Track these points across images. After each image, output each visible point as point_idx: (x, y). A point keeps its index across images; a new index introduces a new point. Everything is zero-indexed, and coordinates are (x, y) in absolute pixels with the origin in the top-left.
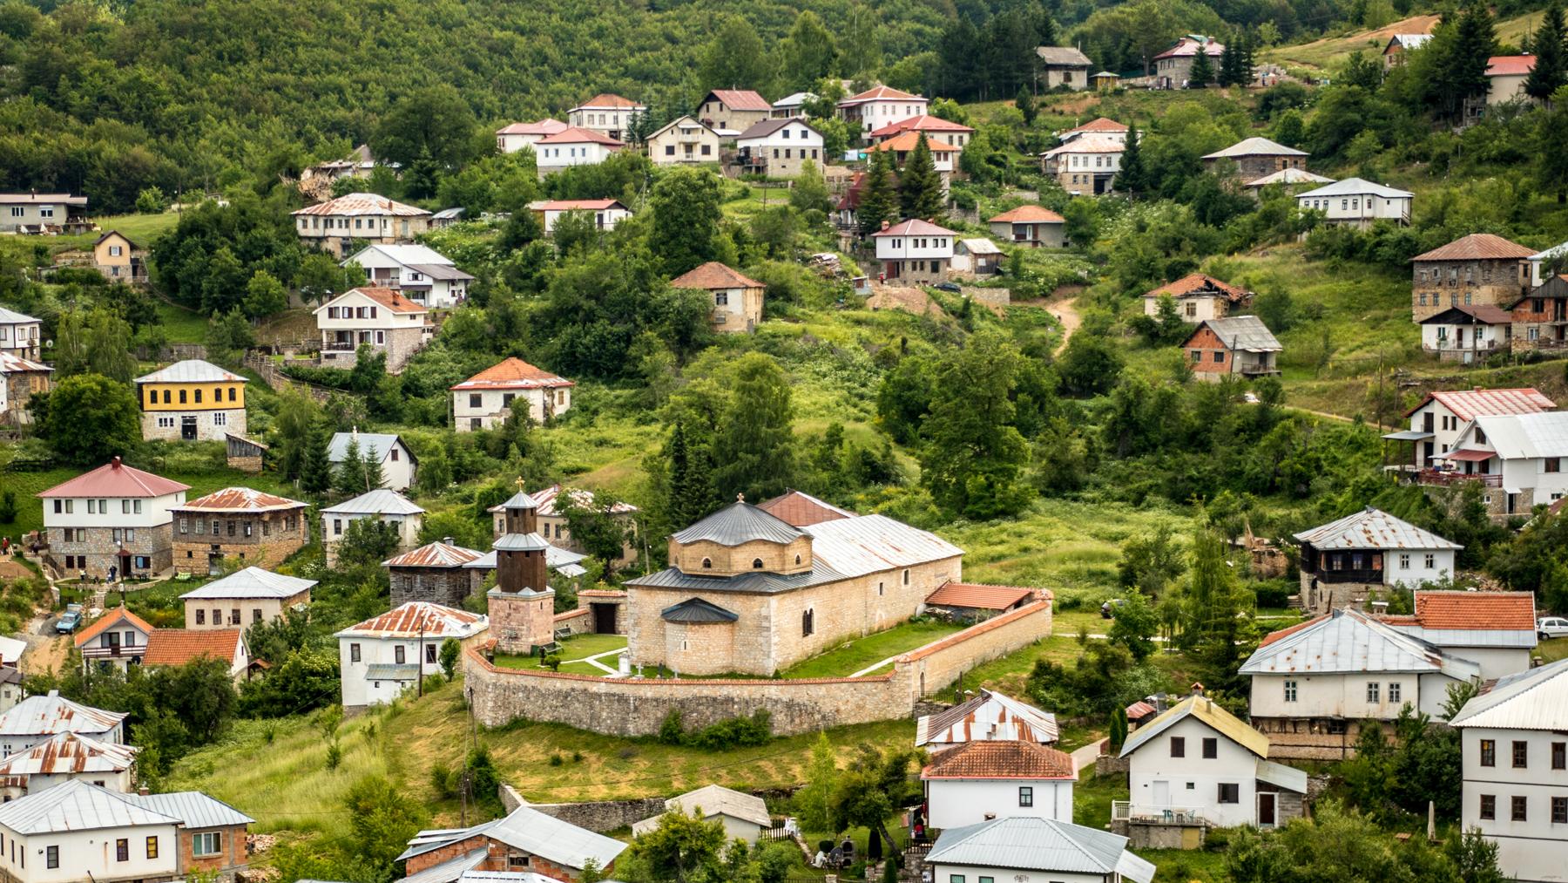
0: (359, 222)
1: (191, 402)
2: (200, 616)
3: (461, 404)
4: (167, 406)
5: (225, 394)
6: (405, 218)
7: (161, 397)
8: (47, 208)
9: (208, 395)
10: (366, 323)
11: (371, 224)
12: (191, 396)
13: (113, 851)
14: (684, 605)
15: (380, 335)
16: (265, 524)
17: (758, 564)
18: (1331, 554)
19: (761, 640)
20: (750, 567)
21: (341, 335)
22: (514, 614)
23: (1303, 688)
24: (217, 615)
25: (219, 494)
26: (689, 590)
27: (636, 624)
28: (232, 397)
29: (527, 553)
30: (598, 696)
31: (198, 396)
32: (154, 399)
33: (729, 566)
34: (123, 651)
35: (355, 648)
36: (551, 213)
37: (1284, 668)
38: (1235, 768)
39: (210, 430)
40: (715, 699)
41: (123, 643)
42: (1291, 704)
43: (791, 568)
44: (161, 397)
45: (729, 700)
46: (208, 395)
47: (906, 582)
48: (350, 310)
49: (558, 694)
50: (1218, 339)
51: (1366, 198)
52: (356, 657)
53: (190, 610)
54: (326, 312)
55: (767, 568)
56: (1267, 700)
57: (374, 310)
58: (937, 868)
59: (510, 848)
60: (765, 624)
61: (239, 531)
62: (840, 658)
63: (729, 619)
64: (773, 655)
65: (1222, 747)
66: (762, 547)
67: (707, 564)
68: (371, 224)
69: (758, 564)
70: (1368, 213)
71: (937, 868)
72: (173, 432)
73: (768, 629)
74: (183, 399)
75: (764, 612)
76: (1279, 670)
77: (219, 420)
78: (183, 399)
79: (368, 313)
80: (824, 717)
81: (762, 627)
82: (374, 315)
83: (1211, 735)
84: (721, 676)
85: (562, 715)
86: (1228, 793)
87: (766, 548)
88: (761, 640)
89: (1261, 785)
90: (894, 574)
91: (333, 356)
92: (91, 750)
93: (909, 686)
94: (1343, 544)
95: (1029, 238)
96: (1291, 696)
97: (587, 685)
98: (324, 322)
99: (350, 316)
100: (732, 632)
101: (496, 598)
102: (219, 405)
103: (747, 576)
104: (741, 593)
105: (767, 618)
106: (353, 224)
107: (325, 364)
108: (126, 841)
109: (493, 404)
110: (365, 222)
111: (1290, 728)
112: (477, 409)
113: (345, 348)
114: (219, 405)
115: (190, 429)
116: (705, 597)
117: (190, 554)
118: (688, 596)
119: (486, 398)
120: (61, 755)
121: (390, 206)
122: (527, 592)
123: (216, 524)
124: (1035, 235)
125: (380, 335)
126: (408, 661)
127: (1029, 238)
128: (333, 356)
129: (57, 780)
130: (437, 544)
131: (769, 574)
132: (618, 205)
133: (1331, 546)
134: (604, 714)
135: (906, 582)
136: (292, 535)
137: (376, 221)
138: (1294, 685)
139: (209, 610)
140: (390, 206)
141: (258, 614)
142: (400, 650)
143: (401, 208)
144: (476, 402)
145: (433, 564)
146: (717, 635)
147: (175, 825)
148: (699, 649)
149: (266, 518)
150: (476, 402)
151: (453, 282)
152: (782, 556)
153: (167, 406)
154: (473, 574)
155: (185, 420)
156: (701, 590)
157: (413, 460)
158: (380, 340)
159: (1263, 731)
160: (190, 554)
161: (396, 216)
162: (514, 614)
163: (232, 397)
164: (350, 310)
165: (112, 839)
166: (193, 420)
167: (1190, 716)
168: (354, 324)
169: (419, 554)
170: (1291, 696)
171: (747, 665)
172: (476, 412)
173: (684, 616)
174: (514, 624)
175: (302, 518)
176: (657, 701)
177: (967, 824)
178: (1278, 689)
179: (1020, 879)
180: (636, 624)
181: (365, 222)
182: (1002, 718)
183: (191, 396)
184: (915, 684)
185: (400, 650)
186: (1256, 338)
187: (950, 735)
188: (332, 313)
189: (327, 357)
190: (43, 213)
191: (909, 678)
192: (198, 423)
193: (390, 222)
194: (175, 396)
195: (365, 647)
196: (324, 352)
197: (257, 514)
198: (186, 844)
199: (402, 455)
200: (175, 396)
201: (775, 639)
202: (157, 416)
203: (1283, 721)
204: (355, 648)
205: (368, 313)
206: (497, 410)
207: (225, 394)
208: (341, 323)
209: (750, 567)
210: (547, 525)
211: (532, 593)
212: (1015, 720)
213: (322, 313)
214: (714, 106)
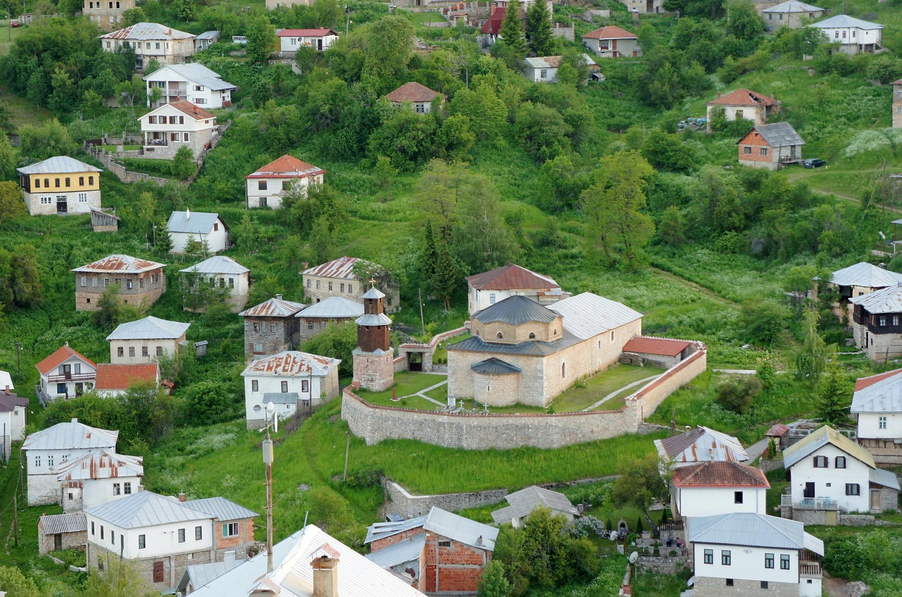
0: (148, 44)
2: (121, 351)
3: (252, 187)
5: (86, 181)
6: (179, 40)
7: (42, 183)
9: (75, 181)
10: (176, 127)
11: (158, 46)
12: (63, 183)
13: (176, 536)
15: (186, 135)
17: (532, 336)
18: (878, 316)
19: (537, 384)
20: (527, 338)
21: (156, 135)
22: (370, 366)
23: (890, 420)
24: (132, 350)
25: (106, 259)
27: (453, 373)
28: (91, 183)
29: (379, 327)
30: (441, 424)
31: (68, 183)
32: (38, 185)
33: (515, 338)
34: (73, 377)
35: (255, 383)
36: (289, 44)
37: (878, 409)
38: (860, 475)
40: (517, 426)
41: (73, 372)
42: (883, 430)
43: (552, 338)
44: (42, 183)
45: (526, 426)
46: (75, 181)
47: (612, 338)
48: (165, 118)
49: (415, 422)
50: (764, 140)
51: (852, 30)
53: (114, 347)
54: (148, 120)
55: (538, 338)
56: (867, 428)
57: (182, 119)
58: (696, 545)
59: (439, 536)
62: (580, 393)
64: (545, 394)
65: (850, 462)
66: (534, 325)
68: (158, 46)
69: (532, 336)
70: (853, 40)
71: (696, 545)
72: (50, 208)
73: (542, 378)
74: (58, 185)
75: (539, 367)
76: (876, 410)
77: (83, 199)
78: (58, 185)
79: (178, 120)
80: (584, 436)
81: (538, 376)
82: (182, 122)
83: (842, 454)
84: (512, 407)
85: (418, 435)
86: (852, 490)
87: (537, 326)
88: (537, 384)
89: (872, 485)
91: (153, 150)
92: (119, 462)
93: (635, 415)
94: (887, 311)
95: (610, 49)
96: (883, 425)
97: (435, 417)
98: (146, 126)
99: (165, 122)
100: (518, 379)
101: (358, 355)
103: (525, 345)
104: (523, 355)
105: (541, 371)
106: (144, 45)
107: (147, 155)
108: (184, 530)
109: (275, 187)
110: (153, 44)
111: (882, 444)
112: (265, 191)
113: (160, 144)
115: (62, 205)
116: (499, 357)
117: (88, 300)
118: (488, 357)
119: (270, 183)
120: (101, 466)
122: (379, 351)
123: (107, 280)
124: (614, 47)
125: (186, 135)
126: (290, 391)
127: (610, 49)
128: (153, 150)
129: (101, 481)
130: (273, 299)
131: (538, 342)
132: (332, 33)
133: (879, 311)
134: (447, 436)
135: (612, 338)
136: (157, 286)
137: (161, 43)
138: (885, 419)
139: (126, 346)
141: (159, 349)
142: (284, 384)
143: (177, 33)
144: (263, 186)
145: (275, 314)
146: (509, 380)
147: (212, 519)
148: (497, 390)
149: (142, 276)
150: (263, 186)
151: (223, 91)
152: (547, 330)
153: (47, 189)
154: (302, 321)
155: (59, 198)
156: (496, 353)
157: (227, 229)
158: (186, 139)
159: (865, 446)
160: (88, 300)
162: (370, 366)
163: (91, 183)
164: (165, 118)
165: (176, 528)
166: (64, 198)
167: (829, 443)
168: (168, 127)
169: (264, 307)
170: (883, 425)
171: (527, 401)
172: (263, 193)
173: (486, 368)
174: (370, 372)
175: (162, 274)
177: (707, 515)
178: (875, 421)
179: (747, 552)
180: (453, 373)
181: (153, 44)
182: (714, 445)
183: (63, 183)
184: (639, 413)
185: (284, 384)
186: (788, 139)
187: (684, 457)
188: (151, 120)
189: (148, 150)
191: (635, 410)
192: (68, 201)
193: (171, 43)
194: (52, 183)
195: (262, 383)
196: (146, 147)
197: (136, 274)
198: (218, 530)
199: (221, 227)
200: (52, 183)
201: (545, 384)
203: (877, 440)
205: (178, 120)
206: (278, 192)
207: (86, 181)
209: (527, 338)
210: (342, 285)
211: (382, 352)
212: (722, 446)
213: (144, 120)
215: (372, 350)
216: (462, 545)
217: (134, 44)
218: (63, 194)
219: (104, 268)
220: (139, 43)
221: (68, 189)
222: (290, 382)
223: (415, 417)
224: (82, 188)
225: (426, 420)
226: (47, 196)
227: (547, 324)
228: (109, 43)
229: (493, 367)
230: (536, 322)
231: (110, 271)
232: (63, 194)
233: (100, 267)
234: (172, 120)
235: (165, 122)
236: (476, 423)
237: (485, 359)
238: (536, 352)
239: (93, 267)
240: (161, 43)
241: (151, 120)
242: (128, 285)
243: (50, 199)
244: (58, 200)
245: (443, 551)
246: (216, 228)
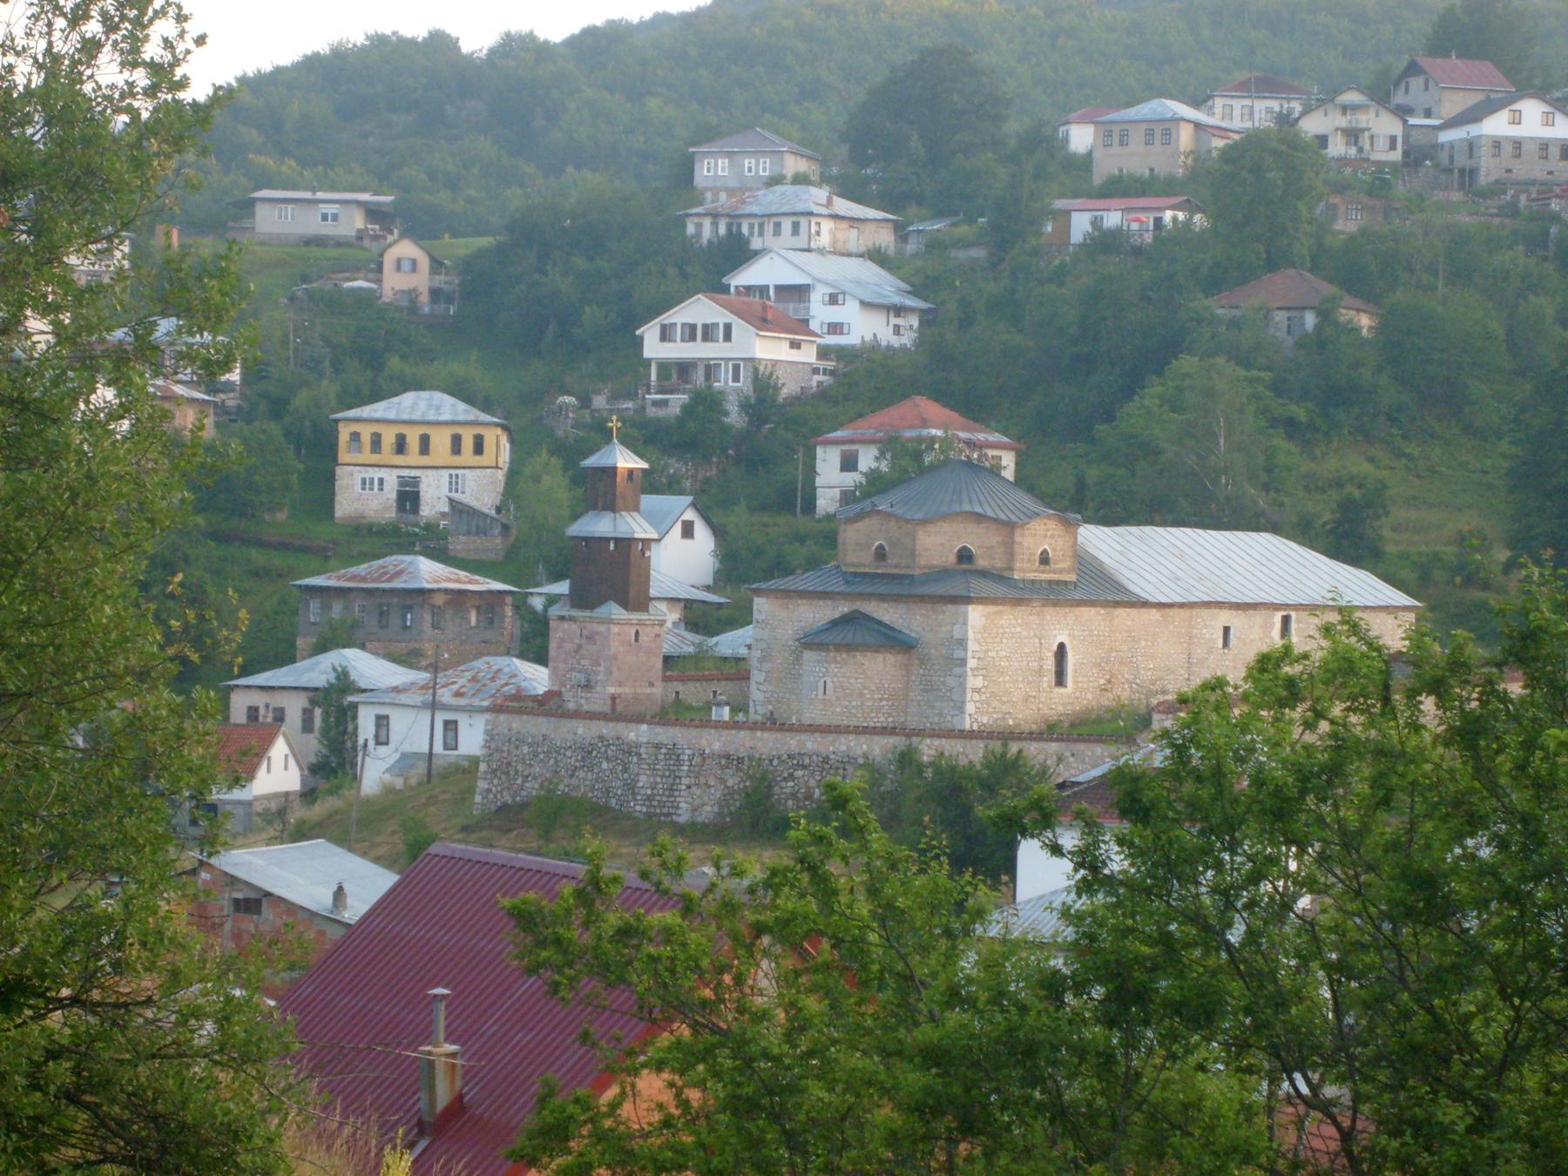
0: (778, 226)
1: (413, 456)
4: (375, 458)
5: (468, 444)
6: (854, 221)
8: (330, 209)
9: (441, 441)
11: (796, 229)
14: (835, 623)
16: (436, 611)
17: (965, 556)
19: (950, 681)
26: (845, 596)
33: (913, 555)
35: (382, 721)
39: (435, 495)
40: (826, 760)
43: (1026, 570)
46: (441, 441)
54: (657, 331)
55: (981, 563)
57: (728, 328)
60: (958, 654)
61: (395, 621)
63: (894, 641)
67: (880, 554)
73: (963, 662)
88: (950, 681)
90: (1258, 617)
98: (654, 348)
101: (562, 618)
102: (457, 460)
104: (922, 599)
114: (457, 460)
118: (844, 608)
121: (830, 201)
137: (803, 222)
140: (830, 201)
151: (898, 310)
152: (1009, 548)
153: (375, 458)
155: (403, 481)
156: (862, 596)
157: (718, 532)
163: (479, 448)
164: (693, 327)
166: (415, 482)
173: (838, 636)
175: (509, 611)
176: (729, 760)
181: (787, 224)
188: (666, 334)
190: (325, 217)
201: (974, 682)
202: (359, 474)
204: (382, 721)
207: (468, 444)
208: (680, 350)
214: (1416, 83)
216: (292, 908)
217: (751, 227)
218: (413, 473)
220: (761, 226)
221: (424, 460)
222: (463, 722)
225: (601, 738)
226: (376, 474)
227: (1009, 527)
228: (699, 226)
229: (852, 634)
230: (980, 518)
232: (413, 473)
233: (354, 578)
234: (708, 333)
235: (693, 338)
236: (717, 746)
237: (837, 615)
238: (960, 591)
239: (339, 578)
240: (803, 222)
241: (666, 334)
242: (404, 619)
243: (381, 481)
244: (401, 484)
245: (243, 926)
246: (688, 531)
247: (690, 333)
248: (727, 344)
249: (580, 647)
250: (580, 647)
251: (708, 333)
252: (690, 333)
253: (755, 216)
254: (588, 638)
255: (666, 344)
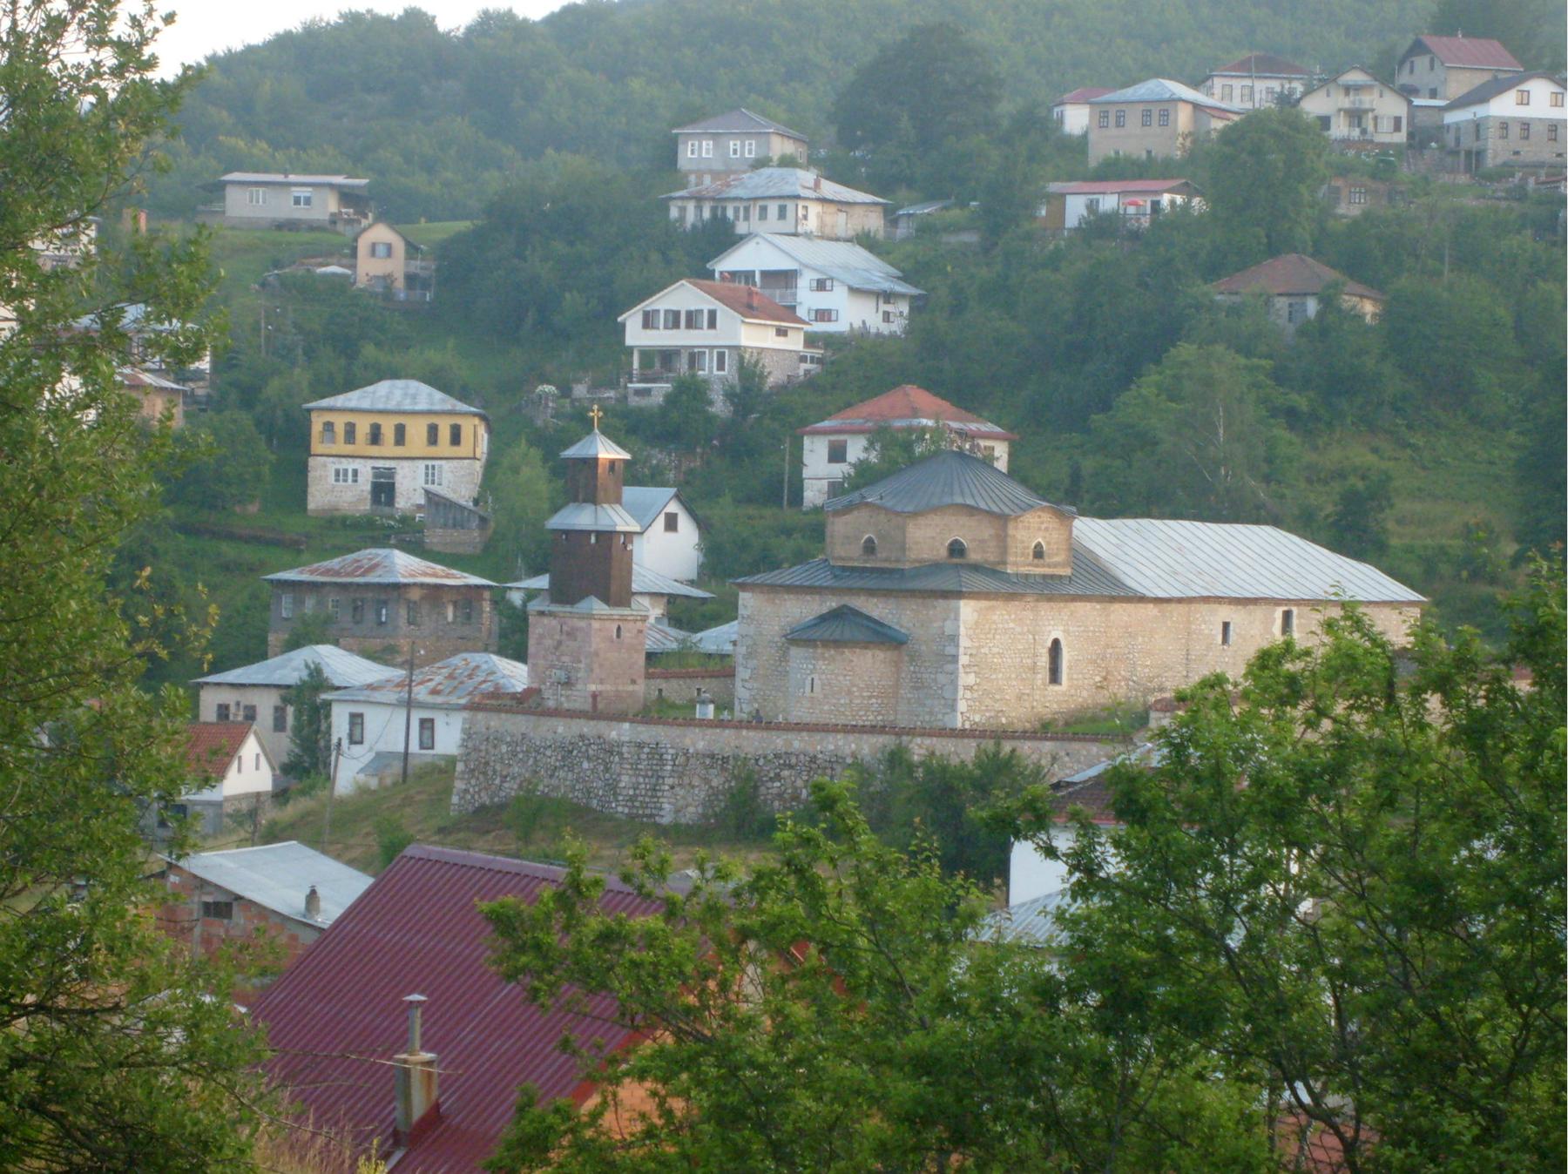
0: (764, 210)
1: (388, 447)
4: (349, 449)
5: (445, 434)
9: (417, 431)
14: (823, 619)
16: (412, 606)
17: (956, 549)
26: (833, 591)
31: (400, 434)
33: (903, 549)
35: (356, 720)
39: (410, 487)
40: (813, 759)
43: (1020, 563)
46: (417, 431)
52: (356, 739)
55: (974, 556)
57: (713, 315)
60: (950, 650)
61: (370, 616)
63: (883, 637)
66: (964, 520)
67: (870, 548)
82: (712, 324)
88: (942, 679)
90: (1259, 612)
98: (636, 335)
101: (542, 613)
104: (912, 593)
114: (433, 451)
115: (384, 489)
118: (832, 603)
121: (817, 185)
137: (790, 205)
151: (888, 296)
152: (1002, 540)
153: (349, 449)
155: (377, 473)
156: (850, 591)
157: (702, 525)
161: (823, 201)
163: (456, 439)
164: (677, 314)
166: (390, 473)
175: (487, 607)
176: (714, 759)
181: (773, 208)
188: (648, 321)
190: (297, 201)
199: (685, 524)
201: (966, 679)
202: (333, 465)
204: (356, 720)
207: (445, 434)
213: (632, 322)
214: (1421, 62)
215: (572, 601)
218: (388, 464)
219: (337, 574)
220: (747, 210)
221: (399, 451)
223: (560, 730)
224: (433, 451)
225: (582, 737)
226: (350, 465)
228: (683, 210)
229: (841, 629)
230: (972, 510)
231: (349, 580)
232: (388, 464)
233: (327, 572)
234: (692, 320)
235: (676, 325)
236: (701, 745)
237: (825, 610)
238: (950, 585)
239: (312, 572)
240: (790, 205)
241: (648, 321)
242: (379, 615)
243: (355, 472)
244: (376, 476)
246: (671, 523)
247: (674, 320)
248: (712, 332)
249: (560, 643)
250: (560, 643)
251: (692, 320)
252: (674, 320)
253: (741, 199)
254: (568, 634)
255: (649, 332)
